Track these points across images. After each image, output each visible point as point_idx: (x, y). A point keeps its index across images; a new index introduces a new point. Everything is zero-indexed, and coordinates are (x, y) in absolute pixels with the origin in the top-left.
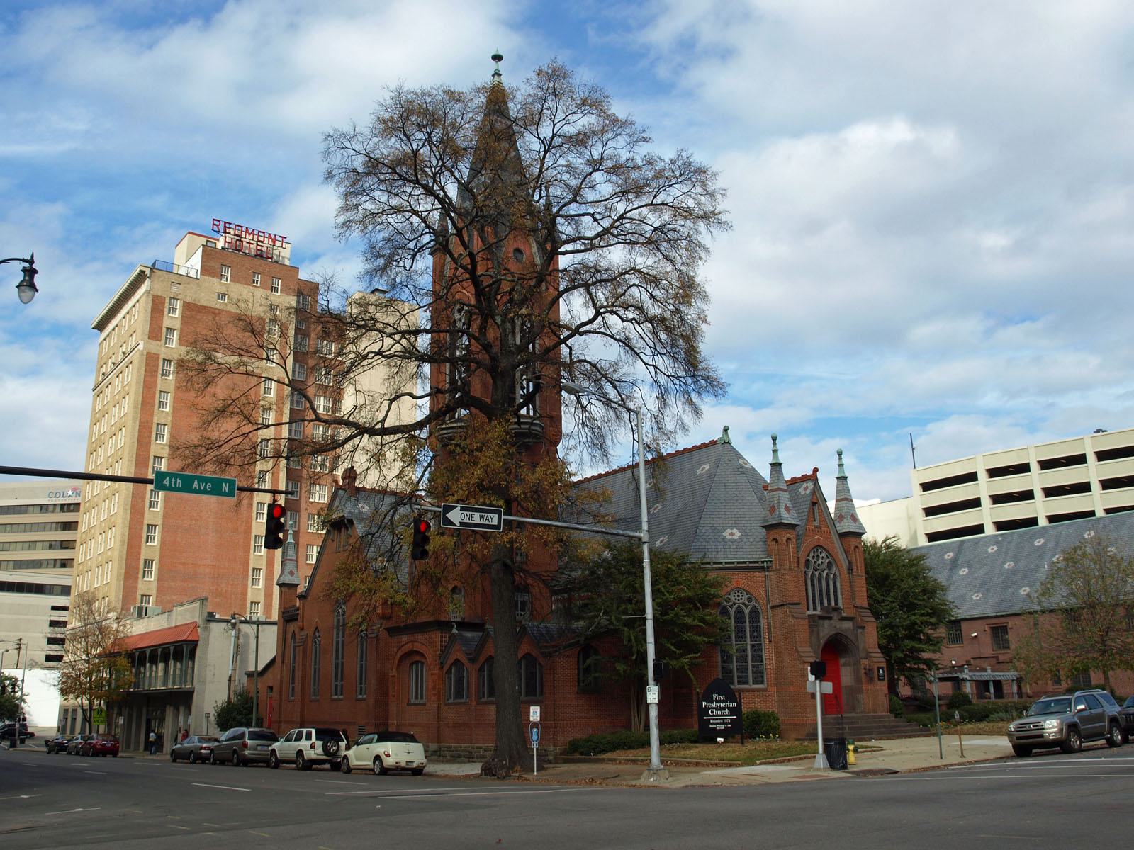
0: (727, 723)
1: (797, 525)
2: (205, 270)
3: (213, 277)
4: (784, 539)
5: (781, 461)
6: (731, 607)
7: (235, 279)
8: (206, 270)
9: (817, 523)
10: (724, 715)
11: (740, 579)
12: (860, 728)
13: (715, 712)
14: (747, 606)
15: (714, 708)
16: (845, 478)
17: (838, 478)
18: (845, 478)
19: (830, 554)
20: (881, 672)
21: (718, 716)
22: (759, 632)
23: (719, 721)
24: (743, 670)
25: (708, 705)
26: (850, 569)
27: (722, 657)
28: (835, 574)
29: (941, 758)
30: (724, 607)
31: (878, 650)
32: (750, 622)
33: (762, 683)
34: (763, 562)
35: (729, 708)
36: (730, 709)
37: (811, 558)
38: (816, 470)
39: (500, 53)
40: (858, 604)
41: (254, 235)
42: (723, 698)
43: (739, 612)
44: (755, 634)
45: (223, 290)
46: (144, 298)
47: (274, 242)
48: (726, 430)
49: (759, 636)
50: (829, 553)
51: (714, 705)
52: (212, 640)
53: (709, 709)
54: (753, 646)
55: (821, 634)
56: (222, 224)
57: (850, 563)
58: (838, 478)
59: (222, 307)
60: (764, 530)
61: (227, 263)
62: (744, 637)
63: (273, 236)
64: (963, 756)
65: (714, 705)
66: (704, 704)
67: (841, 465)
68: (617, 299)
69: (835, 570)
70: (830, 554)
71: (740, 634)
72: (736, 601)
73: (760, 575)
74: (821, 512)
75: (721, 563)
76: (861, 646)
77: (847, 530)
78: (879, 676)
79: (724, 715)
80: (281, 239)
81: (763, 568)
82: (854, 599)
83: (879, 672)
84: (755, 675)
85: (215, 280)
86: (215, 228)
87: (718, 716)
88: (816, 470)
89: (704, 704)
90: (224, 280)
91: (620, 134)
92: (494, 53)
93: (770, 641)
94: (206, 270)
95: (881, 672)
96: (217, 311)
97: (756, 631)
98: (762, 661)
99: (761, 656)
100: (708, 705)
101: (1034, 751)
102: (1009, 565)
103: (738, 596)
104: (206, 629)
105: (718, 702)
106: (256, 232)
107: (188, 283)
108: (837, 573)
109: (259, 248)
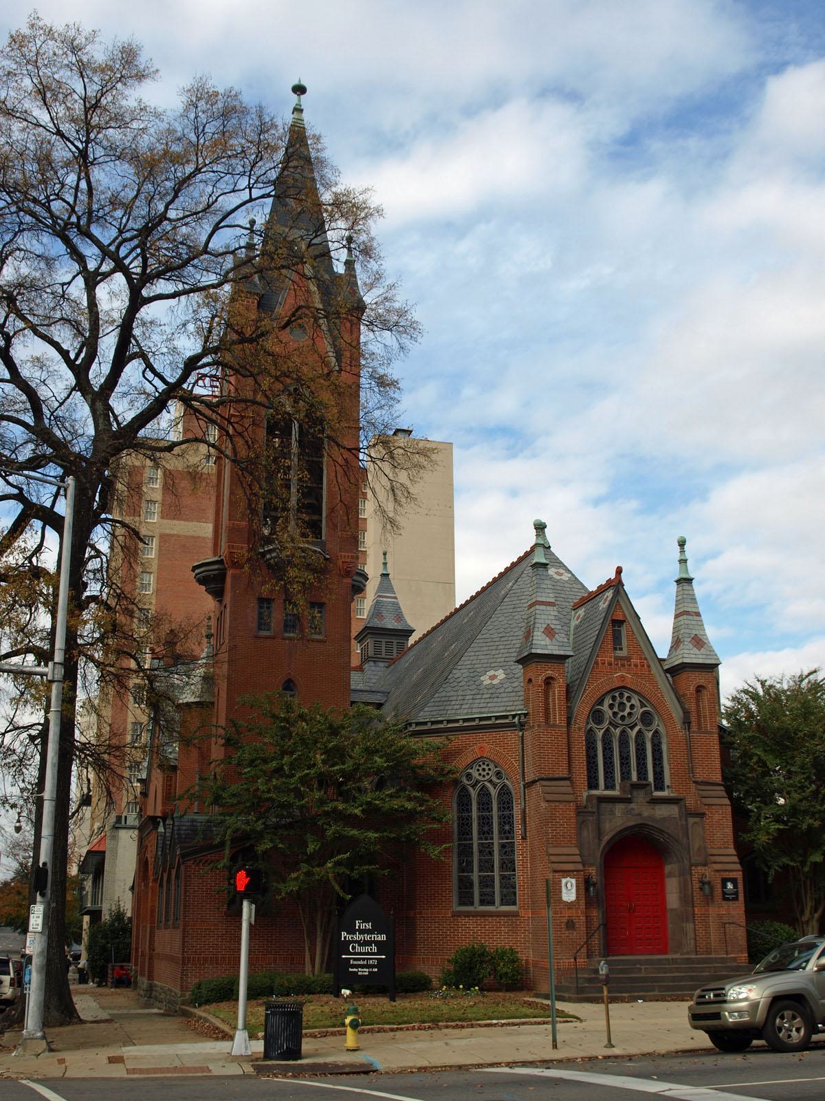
0: (373, 966)
1: (568, 657)
4: (692, 689)
5: (692, 576)
6: (474, 786)
9: (624, 653)
10: (368, 954)
11: (484, 744)
12: (645, 979)
13: (358, 949)
14: (495, 785)
15: (356, 942)
16: (689, 581)
17: (679, 582)
18: (689, 581)
19: (647, 700)
20: (730, 886)
21: (361, 954)
22: (511, 824)
23: (361, 962)
24: (487, 883)
25: (349, 937)
27: (460, 863)
28: (656, 732)
29: (555, 1046)
30: (464, 788)
31: (733, 851)
32: (499, 809)
33: (514, 903)
34: (514, 716)
35: (377, 943)
36: (377, 943)
37: (605, 707)
38: (619, 571)
39: (303, 83)
40: (700, 775)
42: (369, 926)
43: (484, 793)
44: (507, 827)
46: (39, 470)
48: (540, 528)
49: (511, 831)
50: (644, 698)
51: (357, 937)
52: (120, 851)
53: (350, 942)
54: (503, 846)
55: (607, 826)
57: (686, 713)
58: (679, 582)
60: (521, 666)
62: (490, 832)
64: (610, 1045)
65: (357, 937)
66: (344, 934)
67: (683, 561)
69: (657, 724)
70: (647, 700)
71: (486, 829)
72: (480, 778)
73: (512, 737)
74: (631, 635)
75: (457, 721)
76: (696, 844)
77: (680, 661)
78: (724, 893)
79: (368, 954)
81: (512, 725)
82: (692, 770)
83: (724, 886)
84: (505, 891)
87: (361, 954)
88: (619, 571)
89: (344, 934)
91: (71, 70)
92: (296, 82)
93: (524, 838)
95: (730, 886)
97: (507, 820)
98: (514, 870)
99: (513, 862)
100: (349, 937)
101: (755, 1042)
102: (493, 677)
103: (484, 770)
104: (114, 838)
105: (362, 932)
108: (662, 729)
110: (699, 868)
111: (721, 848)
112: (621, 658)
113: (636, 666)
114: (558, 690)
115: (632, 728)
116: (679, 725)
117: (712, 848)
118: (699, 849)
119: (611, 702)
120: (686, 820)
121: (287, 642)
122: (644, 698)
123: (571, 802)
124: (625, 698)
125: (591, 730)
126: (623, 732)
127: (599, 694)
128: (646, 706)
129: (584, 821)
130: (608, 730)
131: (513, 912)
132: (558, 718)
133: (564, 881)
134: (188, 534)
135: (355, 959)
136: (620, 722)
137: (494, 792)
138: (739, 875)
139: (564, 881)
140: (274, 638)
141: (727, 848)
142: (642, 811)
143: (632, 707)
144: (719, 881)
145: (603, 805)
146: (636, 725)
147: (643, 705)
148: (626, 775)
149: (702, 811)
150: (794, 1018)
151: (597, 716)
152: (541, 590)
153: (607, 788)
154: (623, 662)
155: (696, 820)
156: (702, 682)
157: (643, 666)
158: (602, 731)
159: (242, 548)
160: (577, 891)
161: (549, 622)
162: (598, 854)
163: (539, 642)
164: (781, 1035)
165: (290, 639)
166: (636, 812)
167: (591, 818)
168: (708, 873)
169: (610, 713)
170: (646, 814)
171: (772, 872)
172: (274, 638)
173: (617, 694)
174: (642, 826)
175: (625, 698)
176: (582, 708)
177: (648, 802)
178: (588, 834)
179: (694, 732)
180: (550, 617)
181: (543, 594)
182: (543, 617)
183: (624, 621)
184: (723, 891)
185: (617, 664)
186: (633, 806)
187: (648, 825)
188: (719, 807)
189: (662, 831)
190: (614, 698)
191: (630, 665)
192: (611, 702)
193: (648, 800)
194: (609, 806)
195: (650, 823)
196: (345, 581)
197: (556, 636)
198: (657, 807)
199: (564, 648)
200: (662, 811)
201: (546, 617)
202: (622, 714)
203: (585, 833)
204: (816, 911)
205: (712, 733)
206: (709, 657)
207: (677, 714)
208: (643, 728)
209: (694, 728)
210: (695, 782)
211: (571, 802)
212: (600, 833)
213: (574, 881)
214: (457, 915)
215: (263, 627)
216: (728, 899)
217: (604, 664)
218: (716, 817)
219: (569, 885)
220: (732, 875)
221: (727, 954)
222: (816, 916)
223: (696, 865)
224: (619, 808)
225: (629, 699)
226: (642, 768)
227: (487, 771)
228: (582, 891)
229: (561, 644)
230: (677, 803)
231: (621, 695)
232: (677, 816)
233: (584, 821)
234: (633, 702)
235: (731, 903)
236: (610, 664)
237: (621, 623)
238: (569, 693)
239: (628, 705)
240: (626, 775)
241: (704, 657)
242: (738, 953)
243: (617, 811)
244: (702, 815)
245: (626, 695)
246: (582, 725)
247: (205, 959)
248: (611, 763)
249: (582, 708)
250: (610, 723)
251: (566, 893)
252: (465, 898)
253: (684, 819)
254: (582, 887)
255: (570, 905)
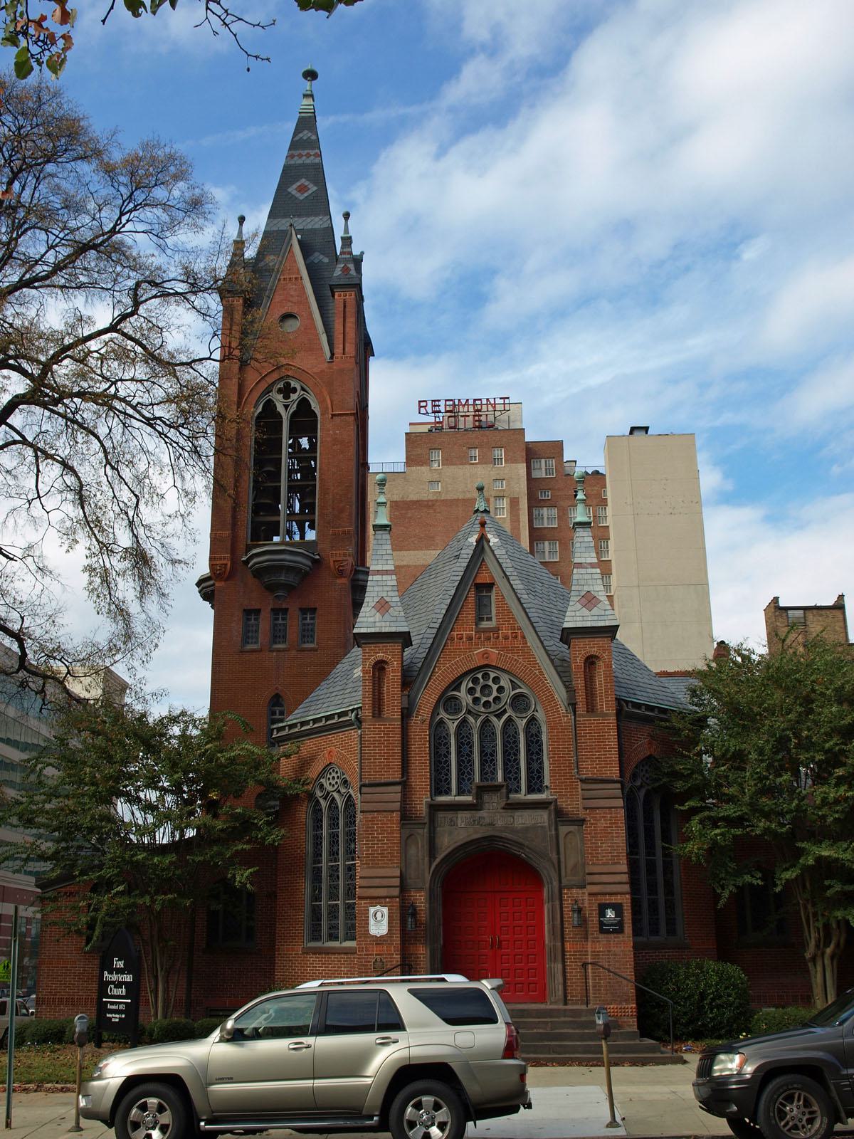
2: (411, 460)
3: (422, 465)
4: (580, 661)
7: (447, 461)
8: (412, 460)
9: (492, 624)
20: (610, 914)
26: (573, 705)
37: (463, 694)
41: (468, 405)
45: (436, 477)
47: (495, 407)
50: (515, 676)
56: (430, 403)
59: (435, 498)
61: (436, 446)
63: (492, 402)
68: (31, 268)
78: (601, 924)
80: (502, 401)
81: (349, 724)
85: (424, 469)
86: (423, 410)
90: (435, 466)
94: (412, 460)
95: (610, 914)
96: (430, 503)
106: (471, 402)
107: (394, 480)
109: (477, 418)
110: (575, 891)
111: (608, 864)
112: (486, 631)
113: (506, 638)
114: (393, 675)
115: (499, 716)
116: (562, 709)
117: (593, 864)
118: (575, 866)
119: (471, 685)
120: (556, 830)
121: (275, 654)
122: (515, 676)
123: (393, 812)
124: (491, 680)
125: (441, 722)
126: (486, 722)
127: (452, 677)
128: (520, 688)
129: (411, 835)
130: (464, 721)
131: (350, 948)
132: (393, 711)
133: (372, 910)
134: (418, 563)
135: (112, 1003)
136: (483, 709)
137: (340, 801)
138: (626, 900)
139: (372, 910)
140: (261, 650)
141: (616, 863)
142: (494, 818)
143: (501, 689)
144: (595, 907)
145: (441, 815)
146: (505, 711)
147: (514, 686)
148: (487, 773)
149: (581, 816)
150: (437, 1107)
151: (448, 701)
152: (378, 557)
153: (530, 790)
154: (487, 635)
155: (572, 828)
156: (594, 651)
157: (516, 637)
158: (525, 721)
159: (224, 558)
160: (390, 922)
161: (384, 594)
162: (428, 877)
163: (365, 619)
164: (411, 1134)
165: (278, 650)
166: (487, 820)
167: (420, 831)
168: (583, 897)
169: (470, 698)
170: (500, 823)
171: (726, 894)
172: (261, 650)
173: (480, 676)
174: (491, 839)
175: (491, 680)
176: (427, 698)
177: (503, 808)
178: (418, 851)
179: (581, 715)
180: (386, 589)
181: (380, 562)
182: (376, 589)
183: (493, 584)
184: (600, 921)
185: (480, 638)
186: (482, 813)
187: (501, 838)
188: (607, 811)
189: (521, 845)
190: (475, 681)
191: (498, 637)
192: (471, 685)
193: (503, 804)
194: (450, 815)
195: (504, 835)
196: (339, 581)
197: (391, 610)
198: (517, 814)
199: (397, 624)
200: (523, 819)
201: (380, 588)
202: (485, 699)
203: (412, 851)
204: (827, 944)
205: (607, 715)
206: (602, 618)
207: (560, 693)
208: (513, 715)
209: (581, 709)
210: (582, 781)
211: (393, 812)
212: (432, 850)
213: (385, 910)
214: (307, 952)
215: (250, 641)
216: (608, 932)
217: (461, 638)
218: (602, 824)
219: (379, 915)
220: (614, 899)
221: (566, 1004)
222: (829, 951)
223: (570, 887)
224: (462, 817)
225: (496, 680)
226: (513, 766)
227: (336, 780)
228: (397, 924)
229: (395, 619)
230: (546, 808)
231: (486, 676)
232: (546, 824)
233: (411, 835)
234: (502, 684)
235: (612, 936)
236: (470, 638)
237: (490, 586)
238: (409, 679)
239: (495, 687)
240: (487, 773)
241: (596, 618)
242: (620, 1003)
243: (459, 821)
244: (582, 822)
245: (492, 675)
246: (427, 716)
247: (61, 1001)
248: (469, 761)
249: (427, 698)
250: (469, 712)
251: (374, 925)
252: (316, 935)
253: (553, 828)
254: (397, 916)
255: (379, 940)
